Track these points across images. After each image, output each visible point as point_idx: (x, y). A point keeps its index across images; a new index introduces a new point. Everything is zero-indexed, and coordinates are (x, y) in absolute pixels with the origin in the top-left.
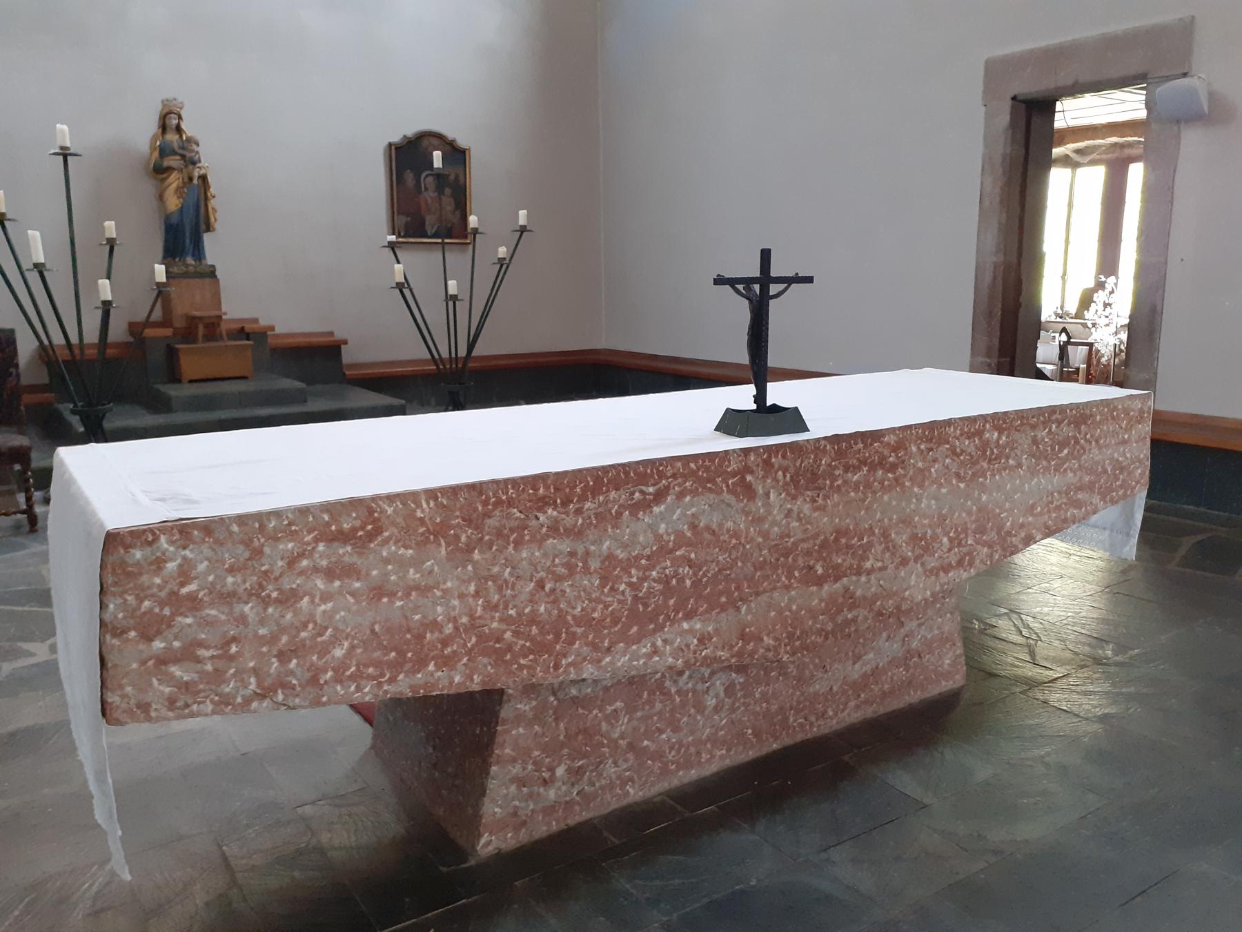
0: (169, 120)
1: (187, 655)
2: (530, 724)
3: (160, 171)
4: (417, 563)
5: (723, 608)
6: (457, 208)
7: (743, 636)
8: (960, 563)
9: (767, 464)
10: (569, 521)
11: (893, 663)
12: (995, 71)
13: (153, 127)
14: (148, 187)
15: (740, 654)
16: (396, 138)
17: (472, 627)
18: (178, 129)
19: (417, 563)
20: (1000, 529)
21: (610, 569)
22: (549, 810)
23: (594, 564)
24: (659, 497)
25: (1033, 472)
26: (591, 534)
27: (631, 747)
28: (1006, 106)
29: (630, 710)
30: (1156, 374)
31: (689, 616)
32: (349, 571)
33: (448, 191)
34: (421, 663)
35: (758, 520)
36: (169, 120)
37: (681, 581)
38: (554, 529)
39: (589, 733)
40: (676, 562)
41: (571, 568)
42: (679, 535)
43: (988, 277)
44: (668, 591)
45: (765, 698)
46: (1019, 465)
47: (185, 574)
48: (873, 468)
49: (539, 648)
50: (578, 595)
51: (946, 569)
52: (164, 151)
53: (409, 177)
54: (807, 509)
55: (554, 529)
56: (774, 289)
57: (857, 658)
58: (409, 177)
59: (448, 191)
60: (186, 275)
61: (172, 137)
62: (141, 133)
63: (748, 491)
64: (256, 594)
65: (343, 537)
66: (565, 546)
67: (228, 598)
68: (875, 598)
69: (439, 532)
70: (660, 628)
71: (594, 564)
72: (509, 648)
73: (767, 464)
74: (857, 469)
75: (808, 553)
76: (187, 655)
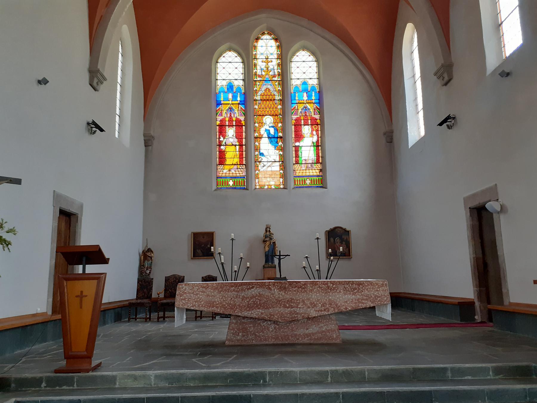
0: (268, 229)
1: (184, 299)
2: (235, 324)
3: (264, 241)
4: (213, 292)
5: (266, 309)
6: (347, 247)
7: (270, 314)
8: (325, 310)
9: (274, 285)
10: (236, 289)
11: (318, 332)
12: (466, 200)
13: (264, 231)
14: (263, 245)
15: (269, 318)
16: (328, 229)
17: (221, 303)
18: (270, 231)
19: (213, 292)
20: (336, 305)
21: (243, 298)
22: (238, 340)
23: (241, 297)
24: (253, 287)
25: (345, 294)
26: (240, 292)
27: (254, 333)
28: (468, 210)
29: (254, 327)
30: (508, 290)
31: (259, 309)
32: (204, 292)
33: (344, 243)
34: (213, 307)
35: (273, 294)
36: (268, 229)
37: (257, 302)
38: (234, 290)
39: (246, 329)
40: (256, 299)
41: (237, 297)
42: (257, 295)
43: (472, 262)
44: (254, 304)
45: (283, 332)
46: (340, 292)
47: (185, 290)
48: (299, 288)
49: (232, 309)
50: (238, 301)
51: (321, 311)
52: (266, 237)
53: (332, 239)
54: (283, 294)
55: (234, 290)
56: (281, 257)
57: (307, 329)
58: (332, 239)
59: (344, 243)
60: (269, 267)
61: (268, 233)
62: (262, 233)
63: (270, 289)
64: (193, 293)
65: (204, 287)
66: (236, 293)
67: (189, 293)
68: (302, 313)
69: (216, 288)
70: (253, 310)
71: (241, 297)
72: (226, 307)
73: (274, 285)
74: (295, 288)
75: (285, 302)
76: (184, 299)
